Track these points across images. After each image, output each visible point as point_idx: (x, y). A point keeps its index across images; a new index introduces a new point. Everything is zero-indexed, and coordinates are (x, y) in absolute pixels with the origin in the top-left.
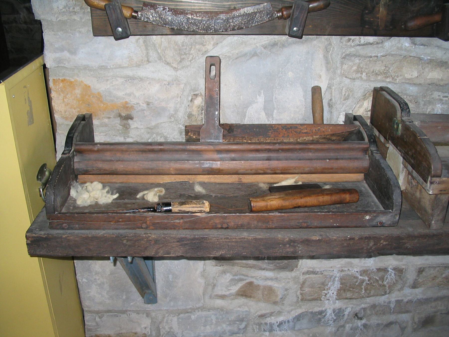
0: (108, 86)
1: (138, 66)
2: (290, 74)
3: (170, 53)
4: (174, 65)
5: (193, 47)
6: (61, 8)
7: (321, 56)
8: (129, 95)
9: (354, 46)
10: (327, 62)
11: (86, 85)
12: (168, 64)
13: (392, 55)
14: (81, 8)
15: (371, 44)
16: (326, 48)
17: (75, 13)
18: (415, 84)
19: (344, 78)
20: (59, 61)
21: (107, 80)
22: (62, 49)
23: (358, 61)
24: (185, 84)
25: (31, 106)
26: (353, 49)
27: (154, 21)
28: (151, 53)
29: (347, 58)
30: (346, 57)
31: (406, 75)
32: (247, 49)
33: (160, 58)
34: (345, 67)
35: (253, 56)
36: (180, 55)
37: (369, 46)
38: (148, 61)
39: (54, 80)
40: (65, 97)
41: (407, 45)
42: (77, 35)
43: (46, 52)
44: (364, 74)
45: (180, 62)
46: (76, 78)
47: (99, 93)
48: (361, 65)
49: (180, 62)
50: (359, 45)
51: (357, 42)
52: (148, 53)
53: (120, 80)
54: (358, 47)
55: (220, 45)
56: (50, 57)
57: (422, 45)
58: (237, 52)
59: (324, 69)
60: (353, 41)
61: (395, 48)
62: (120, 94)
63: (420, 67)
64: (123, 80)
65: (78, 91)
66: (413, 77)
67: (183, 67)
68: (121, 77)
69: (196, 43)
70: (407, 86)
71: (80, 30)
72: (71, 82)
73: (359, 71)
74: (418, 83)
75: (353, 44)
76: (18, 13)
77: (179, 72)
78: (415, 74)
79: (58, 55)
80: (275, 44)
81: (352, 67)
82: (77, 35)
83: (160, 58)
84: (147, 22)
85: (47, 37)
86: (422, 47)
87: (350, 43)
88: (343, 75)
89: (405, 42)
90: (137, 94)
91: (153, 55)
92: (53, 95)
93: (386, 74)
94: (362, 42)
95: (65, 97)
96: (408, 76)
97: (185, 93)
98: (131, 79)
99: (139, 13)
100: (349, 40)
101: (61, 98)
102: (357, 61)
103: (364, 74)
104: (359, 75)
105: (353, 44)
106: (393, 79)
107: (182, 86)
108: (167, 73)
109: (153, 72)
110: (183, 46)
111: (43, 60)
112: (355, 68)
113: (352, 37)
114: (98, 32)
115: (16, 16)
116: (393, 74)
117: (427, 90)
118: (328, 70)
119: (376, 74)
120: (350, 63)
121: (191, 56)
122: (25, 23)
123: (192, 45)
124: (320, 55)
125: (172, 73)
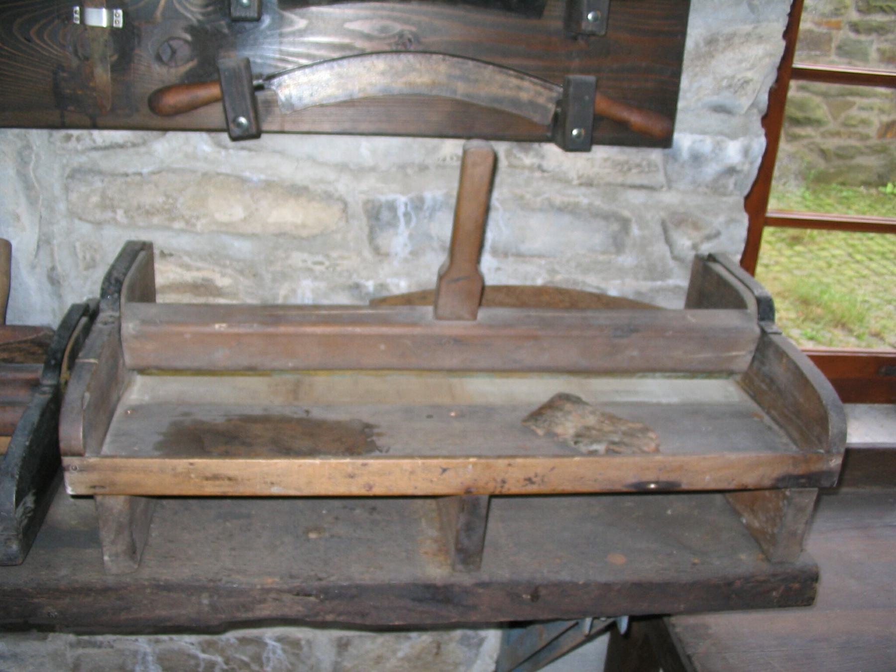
7: (11, 172)
9: (83, 152)
10: (28, 187)
15: (122, 146)
16: (20, 154)
19: (77, 221)
26: (83, 159)
29: (78, 176)
30: (76, 174)
34: (74, 197)
37: (119, 150)
48: (110, 193)
51: (88, 143)
54: (95, 155)
59: (23, 200)
63: (248, 196)
70: (227, 240)
73: (106, 204)
75: (79, 147)
81: (88, 197)
87: (72, 144)
88: (72, 214)
102: (98, 184)
104: (109, 215)
106: (187, 222)
112: (95, 199)
116: (187, 213)
118: (33, 202)
119: (148, 213)
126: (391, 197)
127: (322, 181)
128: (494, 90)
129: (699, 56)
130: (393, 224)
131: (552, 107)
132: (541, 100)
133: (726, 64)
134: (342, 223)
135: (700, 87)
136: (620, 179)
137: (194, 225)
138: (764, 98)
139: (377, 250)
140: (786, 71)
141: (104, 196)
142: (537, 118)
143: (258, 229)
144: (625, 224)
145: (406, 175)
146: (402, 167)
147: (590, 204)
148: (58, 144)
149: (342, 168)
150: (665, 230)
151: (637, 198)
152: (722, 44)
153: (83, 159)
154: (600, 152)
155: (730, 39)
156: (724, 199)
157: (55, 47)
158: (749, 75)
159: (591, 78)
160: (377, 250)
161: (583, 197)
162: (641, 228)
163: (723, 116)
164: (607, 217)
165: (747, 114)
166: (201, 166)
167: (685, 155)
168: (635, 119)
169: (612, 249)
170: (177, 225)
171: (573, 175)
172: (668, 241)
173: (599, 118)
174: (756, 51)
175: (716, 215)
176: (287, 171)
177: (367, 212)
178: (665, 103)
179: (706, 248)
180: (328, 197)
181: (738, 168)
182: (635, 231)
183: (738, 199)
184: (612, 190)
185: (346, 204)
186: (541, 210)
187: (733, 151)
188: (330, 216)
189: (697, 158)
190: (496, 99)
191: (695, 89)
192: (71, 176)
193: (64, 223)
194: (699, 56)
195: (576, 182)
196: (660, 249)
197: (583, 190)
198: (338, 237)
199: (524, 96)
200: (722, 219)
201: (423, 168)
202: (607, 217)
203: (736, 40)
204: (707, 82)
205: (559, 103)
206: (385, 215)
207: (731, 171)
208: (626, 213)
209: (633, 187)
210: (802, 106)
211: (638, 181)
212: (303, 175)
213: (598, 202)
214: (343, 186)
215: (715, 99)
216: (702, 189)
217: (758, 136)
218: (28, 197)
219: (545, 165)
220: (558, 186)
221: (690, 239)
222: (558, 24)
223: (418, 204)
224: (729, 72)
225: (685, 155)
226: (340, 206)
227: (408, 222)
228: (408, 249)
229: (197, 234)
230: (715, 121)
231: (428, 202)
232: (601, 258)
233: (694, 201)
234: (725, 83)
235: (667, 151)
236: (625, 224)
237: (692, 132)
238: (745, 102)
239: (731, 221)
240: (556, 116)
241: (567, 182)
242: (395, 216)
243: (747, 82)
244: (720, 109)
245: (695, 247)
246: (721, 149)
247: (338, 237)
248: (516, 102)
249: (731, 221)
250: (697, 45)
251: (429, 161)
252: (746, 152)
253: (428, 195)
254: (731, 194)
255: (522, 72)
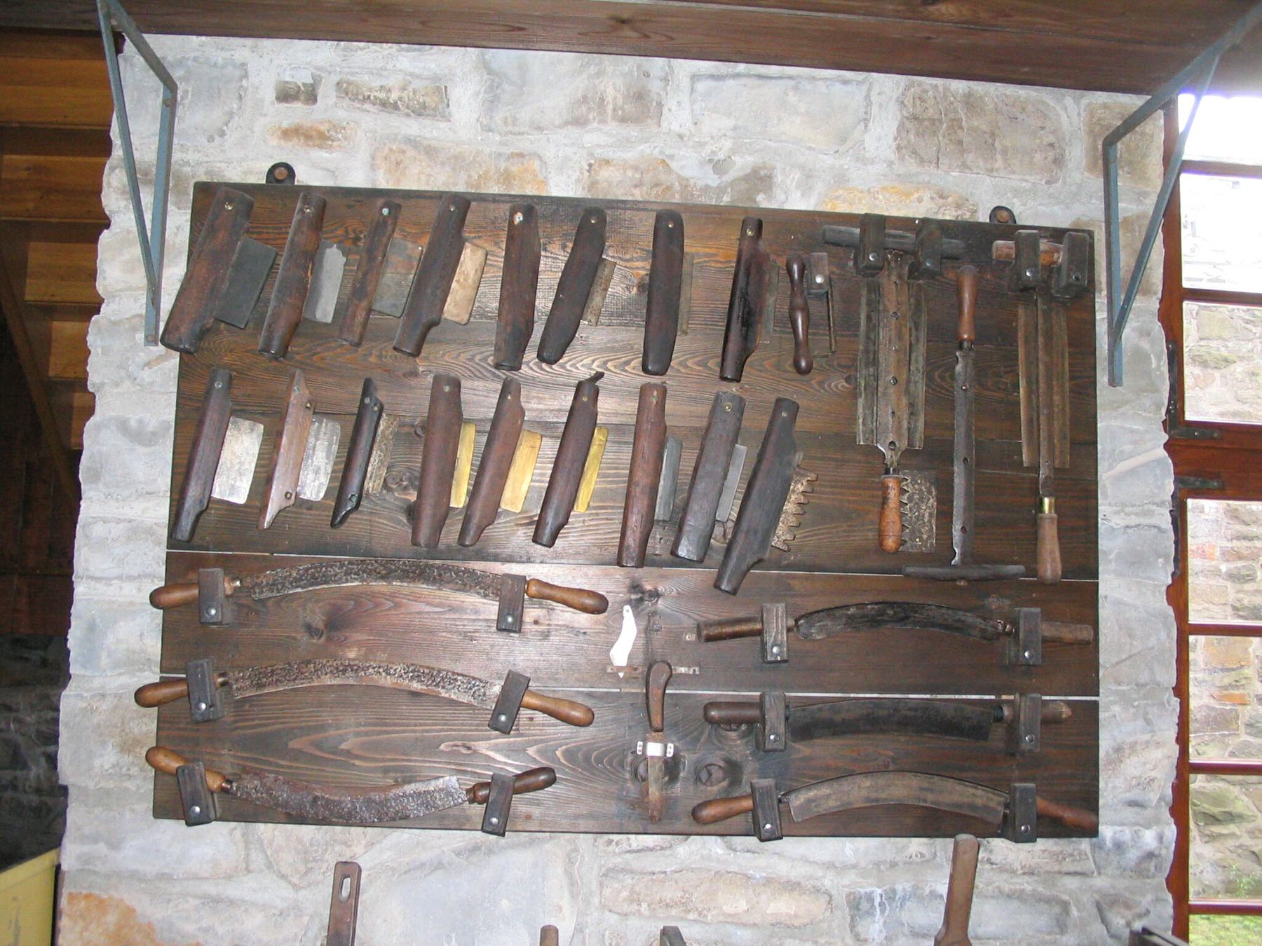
0: (169, 912)
1: (229, 877)
2: (505, 904)
3: (287, 860)
4: (295, 880)
5: (330, 849)
6: (107, 767)
7: (560, 870)
8: (206, 930)
9: (620, 854)
10: (572, 883)
11: (128, 907)
12: (283, 877)
13: (693, 870)
14: (142, 770)
15: (652, 850)
16: (568, 856)
17: (130, 777)
18: (745, 925)
19: (607, 913)
20: (87, 859)
21: (169, 901)
22: (95, 839)
23: (630, 881)
24: (311, 916)
25: (17, 936)
26: (618, 860)
27: (257, 799)
28: (253, 856)
29: (611, 874)
30: (610, 873)
31: (725, 908)
32: (425, 856)
33: (270, 866)
34: (607, 892)
35: (437, 868)
36: (306, 861)
37: (649, 853)
38: (248, 871)
39: (70, 894)
40: (86, 929)
41: (720, 851)
42: (128, 815)
43: (66, 842)
44: (644, 905)
45: (306, 873)
46: (112, 893)
47: (150, 924)
48: (637, 889)
49: (306, 873)
50: (629, 852)
51: (625, 847)
52: (248, 855)
53: (193, 902)
54: (628, 856)
55: (378, 846)
56: (71, 853)
57: (748, 851)
58: (407, 859)
59: (567, 894)
60: (617, 844)
61: (697, 857)
62: (190, 928)
63: (750, 891)
64: (197, 902)
65: (111, 918)
66: (739, 910)
67: (309, 885)
68: (196, 896)
69: (335, 841)
70: (731, 928)
71: (135, 807)
72: (101, 901)
73: (635, 899)
74: (751, 922)
75: (617, 850)
76: (25, 766)
77: (303, 893)
78: (743, 905)
79: (86, 848)
80: (475, 849)
81: (619, 892)
82: (128, 815)
83: (270, 866)
84: (246, 800)
85: (74, 815)
86: (748, 855)
87: (612, 848)
88: (603, 907)
89: (714, 846)
90: (220, 931)
91: (257, 859)
92: (64, 922)
93: (685, 905)
94: (634, 846)
95: (86, 929)
96: (727, 909)
97: (311, 934)
98: (214, 902)
99: (235, 785)
100: (610, 842)
101: (77, 929)
102: (629, 881)
103: (644, 905)
104: (634, 907)
105: (617, 850)
106: (700, 914)
107: (306, 919)
108: (279, 894)
109: (254, 891)
110: (311, 845)
111: (59, 856)
112: (625, 894)
113: (615, 837)
114: (161, 811)
115: (18, 773)
116: (700, 906)
117: (771, 936)
118: (574, 896)
119: (667, 905)
120: (616, 885)
121: (325, 865)
122: (38, 791)
123: (327, 843)
124: (558, 869)
125: (288, 893)
126: (868, 890)
127: (811, 877)
128: (955, 798)
129: (1110, 762)
130: (870, 913)
131: (1001, 809)
132: (992, 804)
133: (1133, 767)
134: (828, 914)
135: (1115, 787)
136: (1056, 868)
137: (706, 916)
138: (1169, 792)
139: (857, 937)
140: (1185, 768)
141: (632, 891)
142: (990, 819)
143: (758, 920)
144: (1065, 906)
145: (880, 871)
146: (877, 864)
147: (1034, 890)
148: (601, 847)
149: (830, 866)
150: (1100, 910)
151: (1072, 883)
152: (1127, 751)
153: (618, 860)
154: (1042, 844)
155: (1133, 746)
156: (1148, 881)
157: (283, 763)
158: (1153, 774)
159: (1031, 785)
160: (857, 937)
161: (1027, 885)
162: (1079, 911)
163: (1136, 809)
164: (1048, 901)
165: (1158, 806)
166: (715, 866)
167: (1109, 844)
168: (1068, 815)
169: (1056, 930)
170: (691, 916)
171: (1017, 866)
172: (1104, 921)
173: (1041, 817)
174: (1156, 754)
175: (1143, 895)
176: (783, 869)
177: (848, 902)
178: (1090, 800)
179: (1138, 926)
180: (817, 891)
181: (1157, 852)
182: (1074, 912)
183: (1161, 879)
184: (1050, 877)
185: (831, 897)
186: (993, 897)
187: (1149, 838)
188: (812, 907)
189: (1119, 846)
190: (960, 806)
191: (1111, 788)
192: (605, 875)
193: (596, 914)
194: (1110, 762)
195: (1020, 872)
196: (1098, 929)
197: (1026, 878)
198: (825, 925)
199: (979, 802)
200: (1149, 897)
201: (893, 865)
202: (1048, 901)
203: (1139, 747)
204: (1119, 782)
205: (1006, 806)
206: (864, 905)
207: (1151, 855)
208: (1065, 897)
209: (1068, 874)
210: (1217, 799)
211: (1072, 869)
212: (796, 872)
213: (1040, 889)
214: (829, 881)
215: (1129, 796)
216: (1128, 873)
217: (1169, 824)
218: (571, 893)
219: (993, 858)
220: (1005, 876)
221: (1123, 917)
222: (1001, 745)
223: (891, 895)
224: (1136, 773)
225: (1109, 844)
226: (825, 898)
227: (883, 911)
228: (884, 934)
229: (707, 924)
230: (1130, 813)
231: (900, 894)
232: (1047, 938)
233: (1122, 884)
234: (1134, 782)
235: (1094, 840)
236: (1065, 906)
237: (1113, 824)
238: (1153, 797)
239: (1158, 900)
240: (1005, 816)
241: (1014, 872)
242: (873, 906)
243: (1153, 780)
244: (1133, 804)
245: (1128, 924)
246: (1139, 837)
247: (825, 925)
248: (973, 807)
249: (1158, 900)
250: (1107, 753)
251: (898, 859)
252: (1160, 838)
253: (899, 888)
254: (1153, 877)
255: (976, 783)
